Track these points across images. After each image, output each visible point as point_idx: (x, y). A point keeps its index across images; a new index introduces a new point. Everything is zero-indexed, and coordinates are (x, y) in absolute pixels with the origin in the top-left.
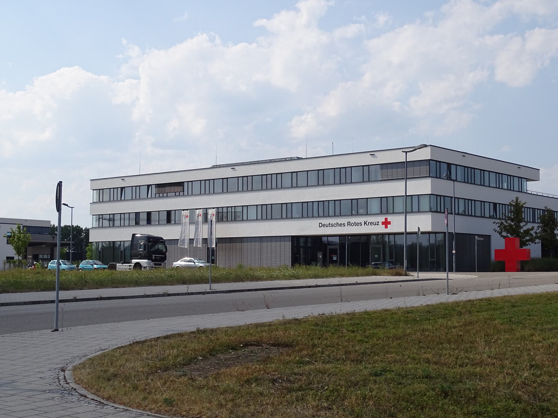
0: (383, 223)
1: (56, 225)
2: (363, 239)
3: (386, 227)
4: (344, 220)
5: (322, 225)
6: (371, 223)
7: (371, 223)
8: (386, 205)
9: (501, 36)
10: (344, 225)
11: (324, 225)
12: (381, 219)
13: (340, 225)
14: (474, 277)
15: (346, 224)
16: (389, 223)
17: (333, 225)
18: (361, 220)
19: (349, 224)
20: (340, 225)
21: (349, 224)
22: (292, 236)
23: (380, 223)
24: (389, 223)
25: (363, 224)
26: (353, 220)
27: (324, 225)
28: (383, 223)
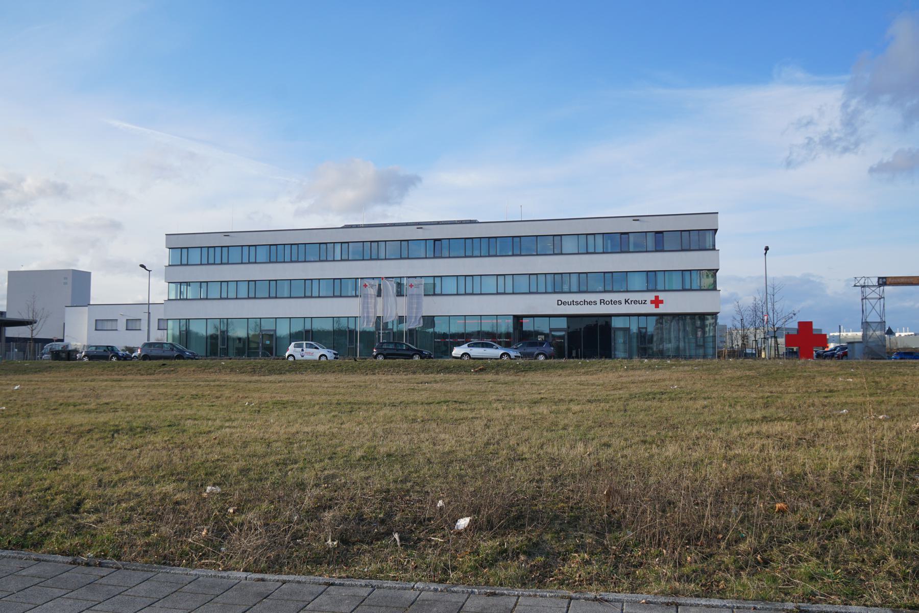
0: (652, 302)
1: (205, 334)
2: (601, 322)
3: (657, 307)
4: (596, 297)
5: (561, 303)
6: (635, 302)
7: (635, 302)
8: (653, 280)
9: (330, 354)
10: (620, 302)
11: (564, 303)
12: (651, 296)
13: (590, 303)
14: (850, 334)
15: (598, 302)
16: (662, 302)
17: (577, 303)
18: (622, 297)
19: (602, 302)
20: (590, 303)
21: (602, 302)
22: (663, 251)
23: (648, 302)
24: (662, 302)
25: (623, 302)
26: (607, 297)
27: (564, 303)
28: (652, 302)
